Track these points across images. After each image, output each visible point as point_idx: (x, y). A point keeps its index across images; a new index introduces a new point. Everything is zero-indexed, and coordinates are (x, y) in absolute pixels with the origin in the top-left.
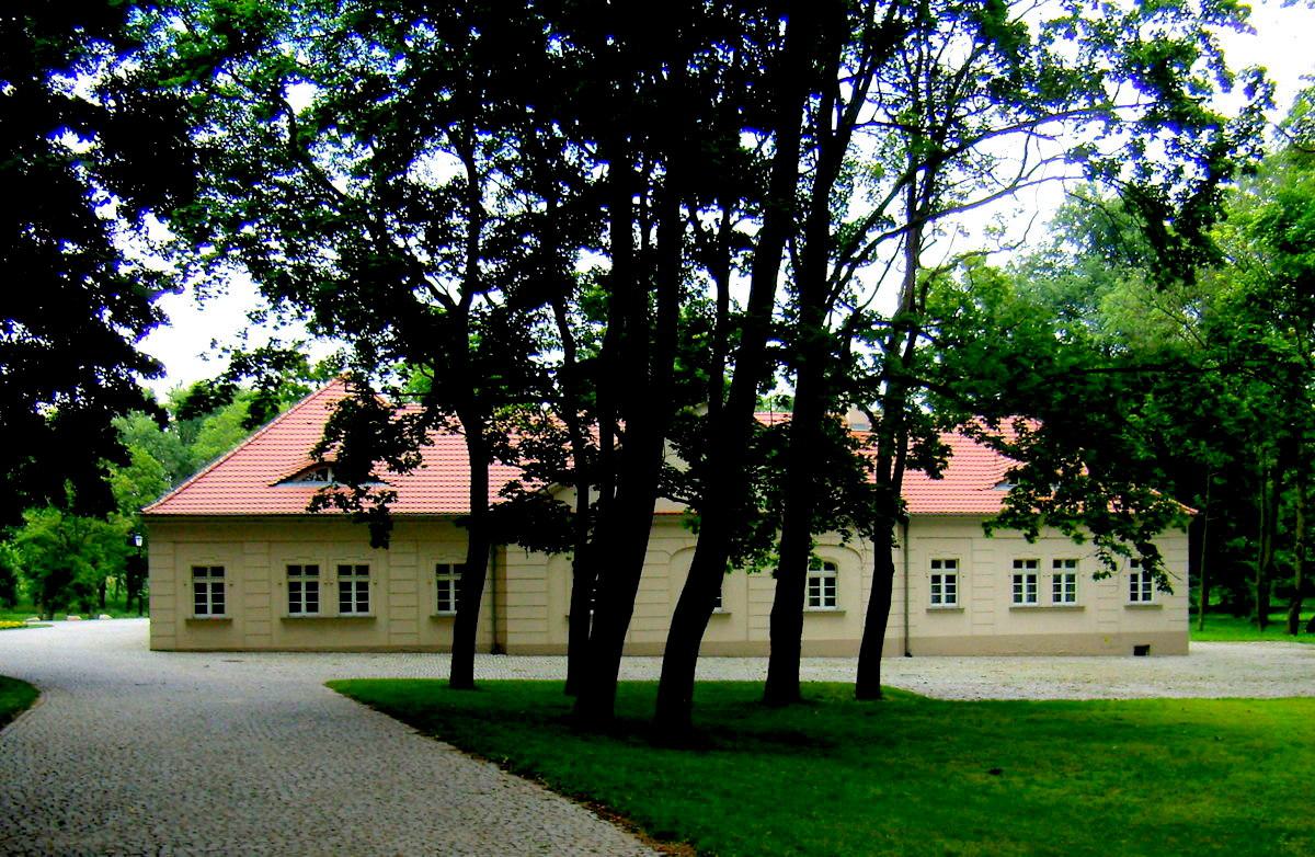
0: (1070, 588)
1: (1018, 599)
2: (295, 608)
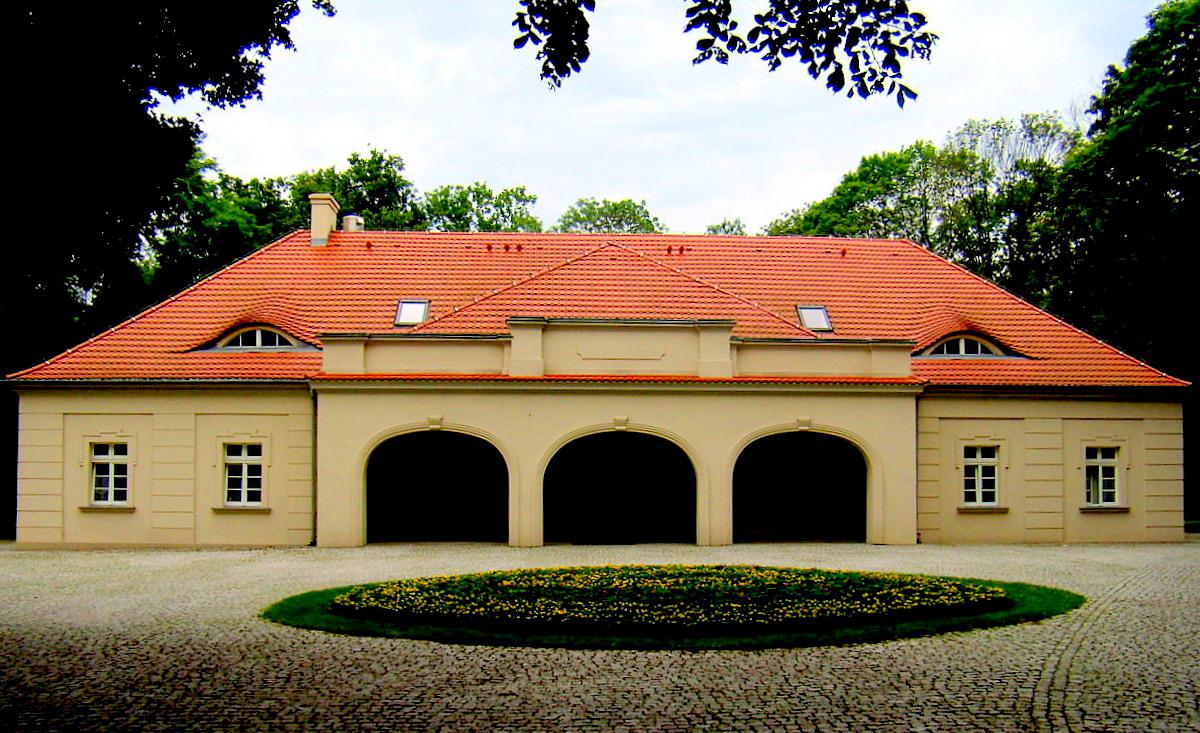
0: (989, 484)
1: (234, 496)
2: (234, 496)
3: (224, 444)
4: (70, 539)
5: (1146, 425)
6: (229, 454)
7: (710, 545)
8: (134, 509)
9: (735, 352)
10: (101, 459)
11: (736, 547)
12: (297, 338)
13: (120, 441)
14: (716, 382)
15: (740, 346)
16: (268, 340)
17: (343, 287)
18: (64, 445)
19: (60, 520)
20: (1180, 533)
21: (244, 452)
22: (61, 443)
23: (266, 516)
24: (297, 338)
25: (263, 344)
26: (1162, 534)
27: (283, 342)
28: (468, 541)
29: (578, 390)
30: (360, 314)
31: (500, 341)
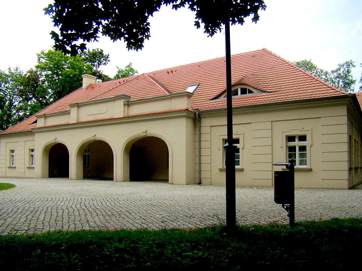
3: (286, 136)
4: (7, 175)
5: (323, 121)
6: (299, 141)
7: (116, 181)
8: (243, 169)
9: (126, 107)
10: (291, 144)
11: (49, 178)
12: (256, 88)
13: (302, 133)
14: (160, 113)
15: (128, 104)
16: (244, 91)
17: (135, 85)
18: (272, 137)
19: (5, 170)
20: (82, 178)
21: (297, 140)
22: (5, 150)
23: (242, 172)
24: (256, 88)
25: (241, 94)
26: (334, 184)
27: (250, 92)
28: (134, 181)
29: (115, 123)
30: (136, 94)
31: (67, 113)
